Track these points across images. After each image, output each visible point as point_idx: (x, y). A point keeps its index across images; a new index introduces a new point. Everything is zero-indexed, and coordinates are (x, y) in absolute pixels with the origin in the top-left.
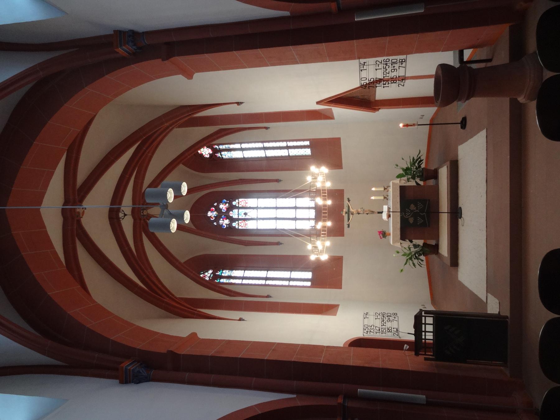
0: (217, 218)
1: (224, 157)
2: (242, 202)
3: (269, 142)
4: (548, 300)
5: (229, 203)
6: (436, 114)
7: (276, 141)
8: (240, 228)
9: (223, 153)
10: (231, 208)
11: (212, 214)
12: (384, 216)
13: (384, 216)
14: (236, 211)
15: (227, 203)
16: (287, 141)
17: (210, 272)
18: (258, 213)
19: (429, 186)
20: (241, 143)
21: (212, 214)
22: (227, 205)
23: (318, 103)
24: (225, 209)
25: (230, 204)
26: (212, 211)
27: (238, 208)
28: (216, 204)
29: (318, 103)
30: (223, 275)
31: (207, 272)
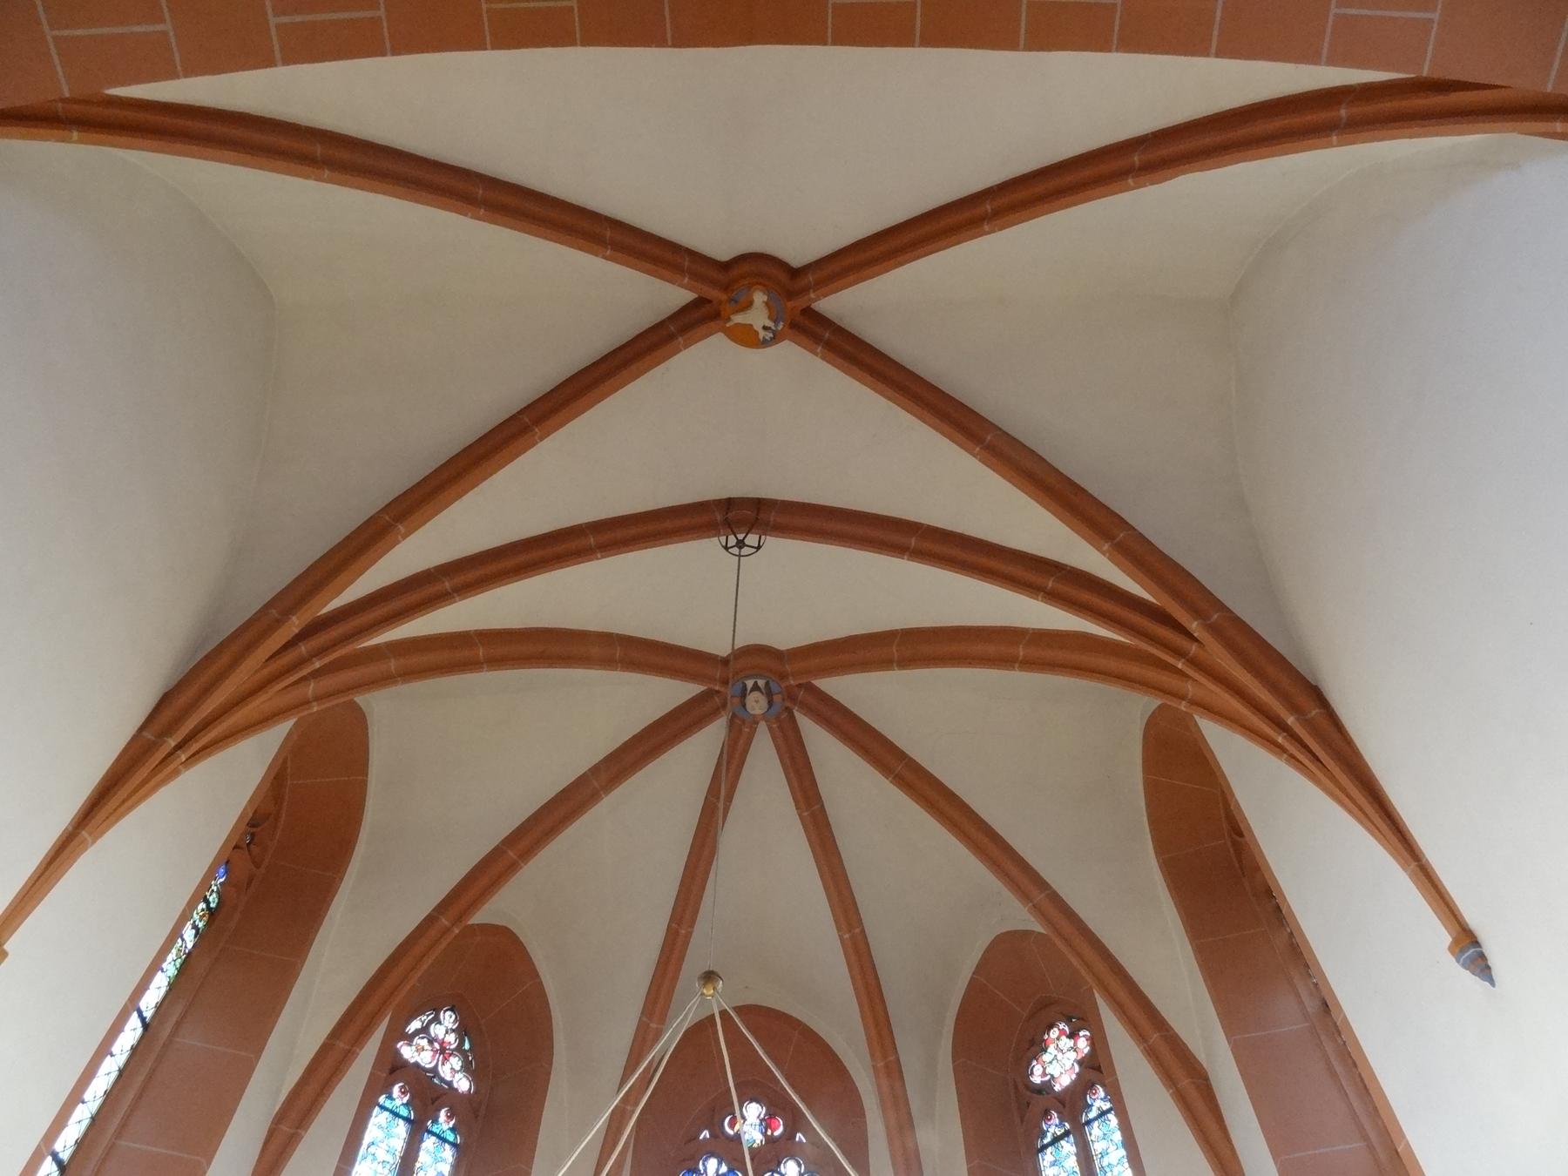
1: (1047, 1158)
10: (427, 1096)
17: (463, 1084)
26: (767, 1123)
30: (429, 1143)
31: (466, 1068)
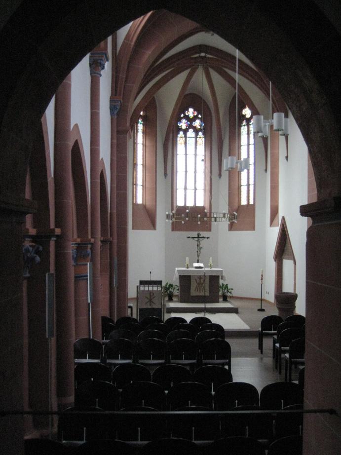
0: (187, 117)
2: (201, 141)
3: (255, 169)
4: (194, 321)
5: (201, 129)
6: (270, 303)
7: (255, 175)
8: (178, 139)
9: (246, 127)
10: (196, 131)
11: (191, 112)
12: (196, 265)
13: (196, 265)
14: (193, 135)
15: (201, 127)
16: (254, 185)
18: (191, 154)
19: (75, 400)
20: (254, 144)
21: (191, 112)
22: (199, 127)
23: (283, 218)
24: (195, 125)
25: (200, 130)
26: (193, 113)
27: (196, 137)
28: (200, 116)
29: (283, 218)
